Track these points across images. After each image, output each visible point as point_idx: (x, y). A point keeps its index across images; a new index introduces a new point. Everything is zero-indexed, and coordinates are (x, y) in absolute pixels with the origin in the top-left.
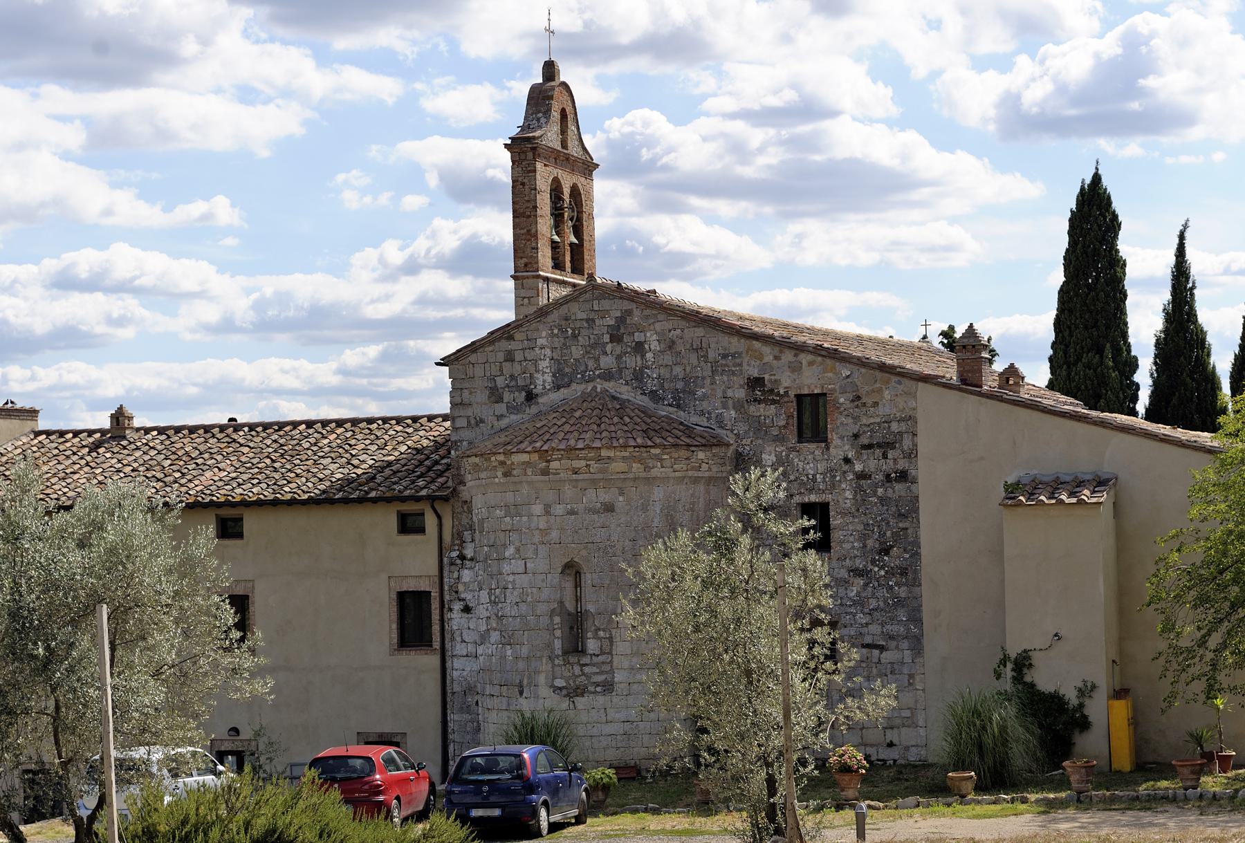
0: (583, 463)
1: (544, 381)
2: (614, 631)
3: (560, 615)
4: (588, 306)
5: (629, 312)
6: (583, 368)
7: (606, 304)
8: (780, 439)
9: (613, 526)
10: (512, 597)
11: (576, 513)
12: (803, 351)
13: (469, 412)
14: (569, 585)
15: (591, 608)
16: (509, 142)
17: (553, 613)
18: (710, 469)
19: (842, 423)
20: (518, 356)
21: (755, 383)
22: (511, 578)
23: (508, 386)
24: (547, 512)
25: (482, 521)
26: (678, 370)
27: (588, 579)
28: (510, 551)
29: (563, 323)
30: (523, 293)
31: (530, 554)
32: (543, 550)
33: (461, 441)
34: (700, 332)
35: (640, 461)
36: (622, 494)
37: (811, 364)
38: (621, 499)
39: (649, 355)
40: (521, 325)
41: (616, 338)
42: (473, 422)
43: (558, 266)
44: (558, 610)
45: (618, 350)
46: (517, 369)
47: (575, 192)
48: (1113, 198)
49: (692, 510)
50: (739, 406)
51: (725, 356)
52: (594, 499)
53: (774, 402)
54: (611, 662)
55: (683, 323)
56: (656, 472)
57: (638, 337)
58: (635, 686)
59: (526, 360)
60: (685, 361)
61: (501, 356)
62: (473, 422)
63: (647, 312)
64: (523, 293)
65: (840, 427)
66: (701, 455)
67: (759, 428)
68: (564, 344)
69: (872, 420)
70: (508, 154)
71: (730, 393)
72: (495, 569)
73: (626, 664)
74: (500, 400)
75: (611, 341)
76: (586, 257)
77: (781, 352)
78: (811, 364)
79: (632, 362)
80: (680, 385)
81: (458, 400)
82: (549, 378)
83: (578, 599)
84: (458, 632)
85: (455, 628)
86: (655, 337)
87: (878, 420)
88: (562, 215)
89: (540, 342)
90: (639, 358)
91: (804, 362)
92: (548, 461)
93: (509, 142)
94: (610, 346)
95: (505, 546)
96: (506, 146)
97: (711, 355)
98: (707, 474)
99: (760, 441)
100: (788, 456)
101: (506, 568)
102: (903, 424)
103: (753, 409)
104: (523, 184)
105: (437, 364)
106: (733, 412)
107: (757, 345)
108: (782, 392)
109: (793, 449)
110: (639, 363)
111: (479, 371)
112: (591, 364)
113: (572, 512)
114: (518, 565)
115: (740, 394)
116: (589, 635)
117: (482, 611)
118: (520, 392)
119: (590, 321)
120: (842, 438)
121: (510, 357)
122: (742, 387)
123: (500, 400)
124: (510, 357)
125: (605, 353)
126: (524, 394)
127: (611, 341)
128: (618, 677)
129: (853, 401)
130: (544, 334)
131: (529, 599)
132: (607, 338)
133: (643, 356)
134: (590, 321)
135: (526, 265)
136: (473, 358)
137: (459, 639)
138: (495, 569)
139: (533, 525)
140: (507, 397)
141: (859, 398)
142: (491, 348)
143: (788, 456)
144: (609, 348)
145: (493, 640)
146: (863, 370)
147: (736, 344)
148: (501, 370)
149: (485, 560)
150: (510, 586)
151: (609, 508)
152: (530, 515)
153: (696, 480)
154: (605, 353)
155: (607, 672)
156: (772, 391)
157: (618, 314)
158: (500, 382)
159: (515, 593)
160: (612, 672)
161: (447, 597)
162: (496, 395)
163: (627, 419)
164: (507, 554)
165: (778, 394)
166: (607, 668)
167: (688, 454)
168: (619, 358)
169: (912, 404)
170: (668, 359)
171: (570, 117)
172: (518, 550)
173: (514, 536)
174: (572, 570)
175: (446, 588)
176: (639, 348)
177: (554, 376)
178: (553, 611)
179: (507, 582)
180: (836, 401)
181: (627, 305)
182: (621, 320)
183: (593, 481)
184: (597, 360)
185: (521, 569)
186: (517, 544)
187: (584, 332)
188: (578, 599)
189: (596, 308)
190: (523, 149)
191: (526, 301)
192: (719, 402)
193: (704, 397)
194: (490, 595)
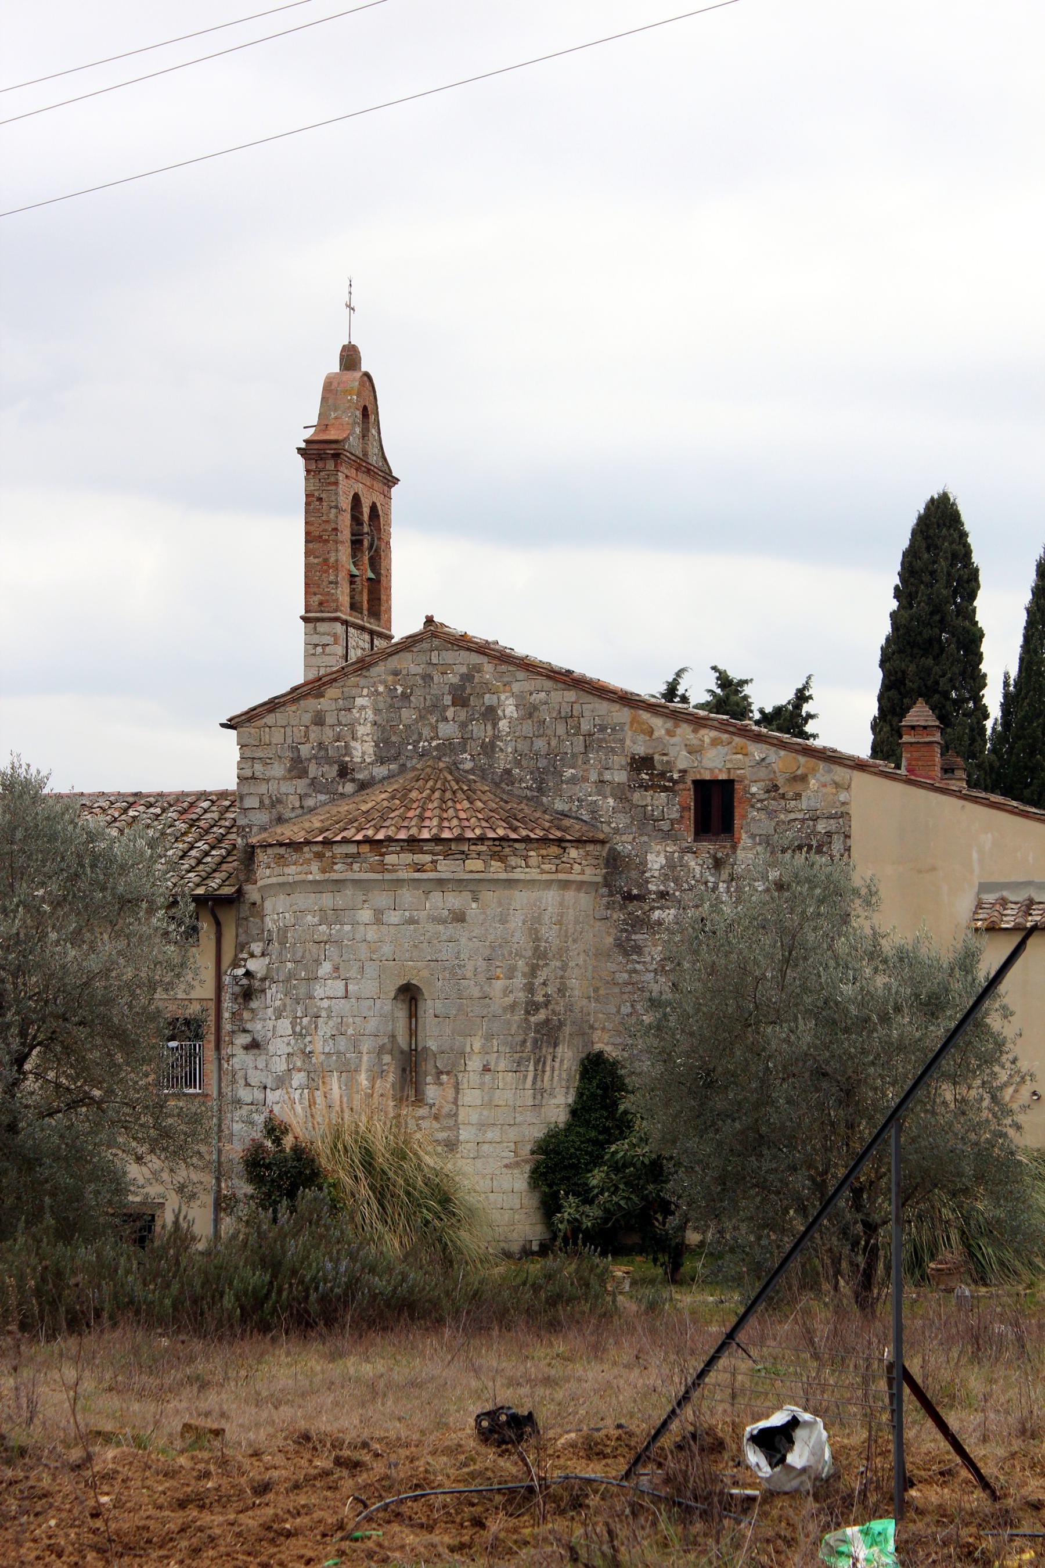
0: (428, 858)
1: (364, 753)
2: (460, 1075)
3: (391, 1053)
4: (424, 658)
5: (478, 668)
6: (415, 737)
7: (449, 656)
8: (669, 835)
9: (463, 941)
10: (325, 1028)
11: (417, 922)
12: (705, 726)
13: (263, 789)
14: (401, 1014)
15: (432, 1045)
16: (303, 445)
17: (381, 1050)
18: (583, 873)
19: (753, 818)
20: (330, 720)
21: (641, 763)
22: (325, 1003)
23: (315, 757)
24: (378, 921)
25: (283, 931)
26: (540, 744)
27: (429, 1007)
28: (326, 968)
29: (390, 678)
30: (316, 639)
31: (353, 973)
32: (371, 969)
33: (250, 826)
34: (571, 695)
35: (502, 859)
36: (475, 900)
37: (715, 742)
38: (474, 905)
39: (503, 725)
40: (335, 680)
41: (460, 700)
42: (267, 802)
43: (354, 607)
44: (389, 1046)
45: (463, 715)
46: (328, 734)
47: (374, 508)
48: (982, 578)
49: (559, 923)
50: (622, 794)
51: (603, 729)
52: (440, 905)
53: (665, 789)
54: (456, 1115)
55: (548, 684)
56: (517, 875)
57: (489, 699)
58: (485, 1147)
59: (340, 724)
60: (549, 732)
61: (307, 718)
62: (267, 802)
63: (503, 668)
64: (316, 639)
65: (752, 822)
66: (573, 853)
67: (646, 821)
68: (391, 706)
69: (792, 816)
70: (301, 461)
71: (607, 776)
72: (302, 991)
73: (474, 1118)
74: (303, 773)
75: (454, 704)
76: (383, 597)
77: (676, 726)
78: (715, 742)
79: (479, 730)
80: (542, 763)
81: (248, 773)
82: (369, 748)
83: (413, 1033)
84: (241, 1074)
85: (237, 1067)
86: (511, 701)
87: (800, 816)
88: (361, 542)
89: (360, 701)
90: (489, 727)
91: (707, 740)
92: (383, 855)
93: (303, 445)
94: (452, 709)
95: (318, 962)
96: (299, 449)
97: (585, 727)
98: (579, 878)
99: (645, 838)
100: (681, 858)
101: (319, 991)
102: (832, 821)
103: (637, 797)
104: (320, 499)
105: (223, 725)
106: (611, 801)
107: (645, 716)
108: (676, 776)
109: (689, 850)
110: (490, 732)
111: (277, 737)
112: (426, 732)
113: (412, 921)
114: (337, 987)
115: (620, 777)
116: (429, 1079)
117: (280, 1046)
118: (331, 765)
119: (427, 678)
120: (753, 836)
121: (319, 720)
122: (622, 768)
123: (303, 773)
124: (319, 720)
125: (446, 720)
126: (336, 767)
127: (454, 704)
128: (464, 1134)
129: (768, 791)
130: (365, 692)
131: (350, 1031)
132: (448, 700)
133: (495, 725)
134: (427, 678)
135: (321, 604)
136: (270, 719)
137: (242, 1082)
138: (302, 991)
139: (358, 936)
140: (313, 770)
141: (776, 787)
142: (294, 708)
143: (681, 858)
144: (450, 713)
145: (295, 1083)
146: (782, 753)
147: (621, 715)
148: (306, 735)
149: (288, 980)
150: (324, 1014)
151: (459, 917)
152: (355, 924)
153: (565, 885)
154: (446, 720)
155: (449, 1128)
156: (662, 775)
157: (464, 670)
158: (305, 750)
159: (331, 1023)
160: (456, 1126)
161: (227, 1027)
162: (298, 768)
163: (479, 804)
164: (321, 973)
165: (671, 779)
166: (452, 1122)
167: (560, 851)
168: (463, 725)
169: (843, 797)
170: (527, 728)
171: (372, 418)
172: (336, 969)
173: (332, 950)
174: (409, 995)
175: (226, 1015)
176: (491, 714)
177: (377, 746)
178: (382, 1047)
179: (320, 1008)
180: (746, 790)
181: (475, 659)
182: (467, 678)
183: (441, 882)
184: (435, 728)
185: (341, 993)
186: (337, 959)
187: (418, 692)
188: (413, 1033)
189: (435, 661)
190: (320, 454)
191: (319, 649)
192: (592, 790)
193: (573, 780)
194: (293, 1025)
